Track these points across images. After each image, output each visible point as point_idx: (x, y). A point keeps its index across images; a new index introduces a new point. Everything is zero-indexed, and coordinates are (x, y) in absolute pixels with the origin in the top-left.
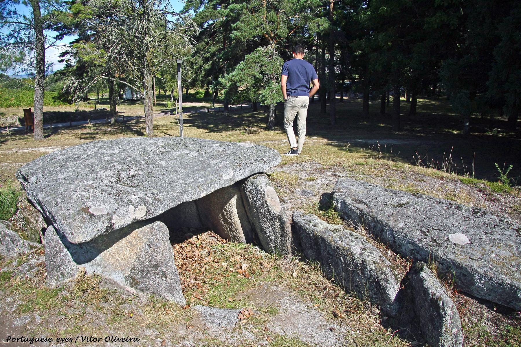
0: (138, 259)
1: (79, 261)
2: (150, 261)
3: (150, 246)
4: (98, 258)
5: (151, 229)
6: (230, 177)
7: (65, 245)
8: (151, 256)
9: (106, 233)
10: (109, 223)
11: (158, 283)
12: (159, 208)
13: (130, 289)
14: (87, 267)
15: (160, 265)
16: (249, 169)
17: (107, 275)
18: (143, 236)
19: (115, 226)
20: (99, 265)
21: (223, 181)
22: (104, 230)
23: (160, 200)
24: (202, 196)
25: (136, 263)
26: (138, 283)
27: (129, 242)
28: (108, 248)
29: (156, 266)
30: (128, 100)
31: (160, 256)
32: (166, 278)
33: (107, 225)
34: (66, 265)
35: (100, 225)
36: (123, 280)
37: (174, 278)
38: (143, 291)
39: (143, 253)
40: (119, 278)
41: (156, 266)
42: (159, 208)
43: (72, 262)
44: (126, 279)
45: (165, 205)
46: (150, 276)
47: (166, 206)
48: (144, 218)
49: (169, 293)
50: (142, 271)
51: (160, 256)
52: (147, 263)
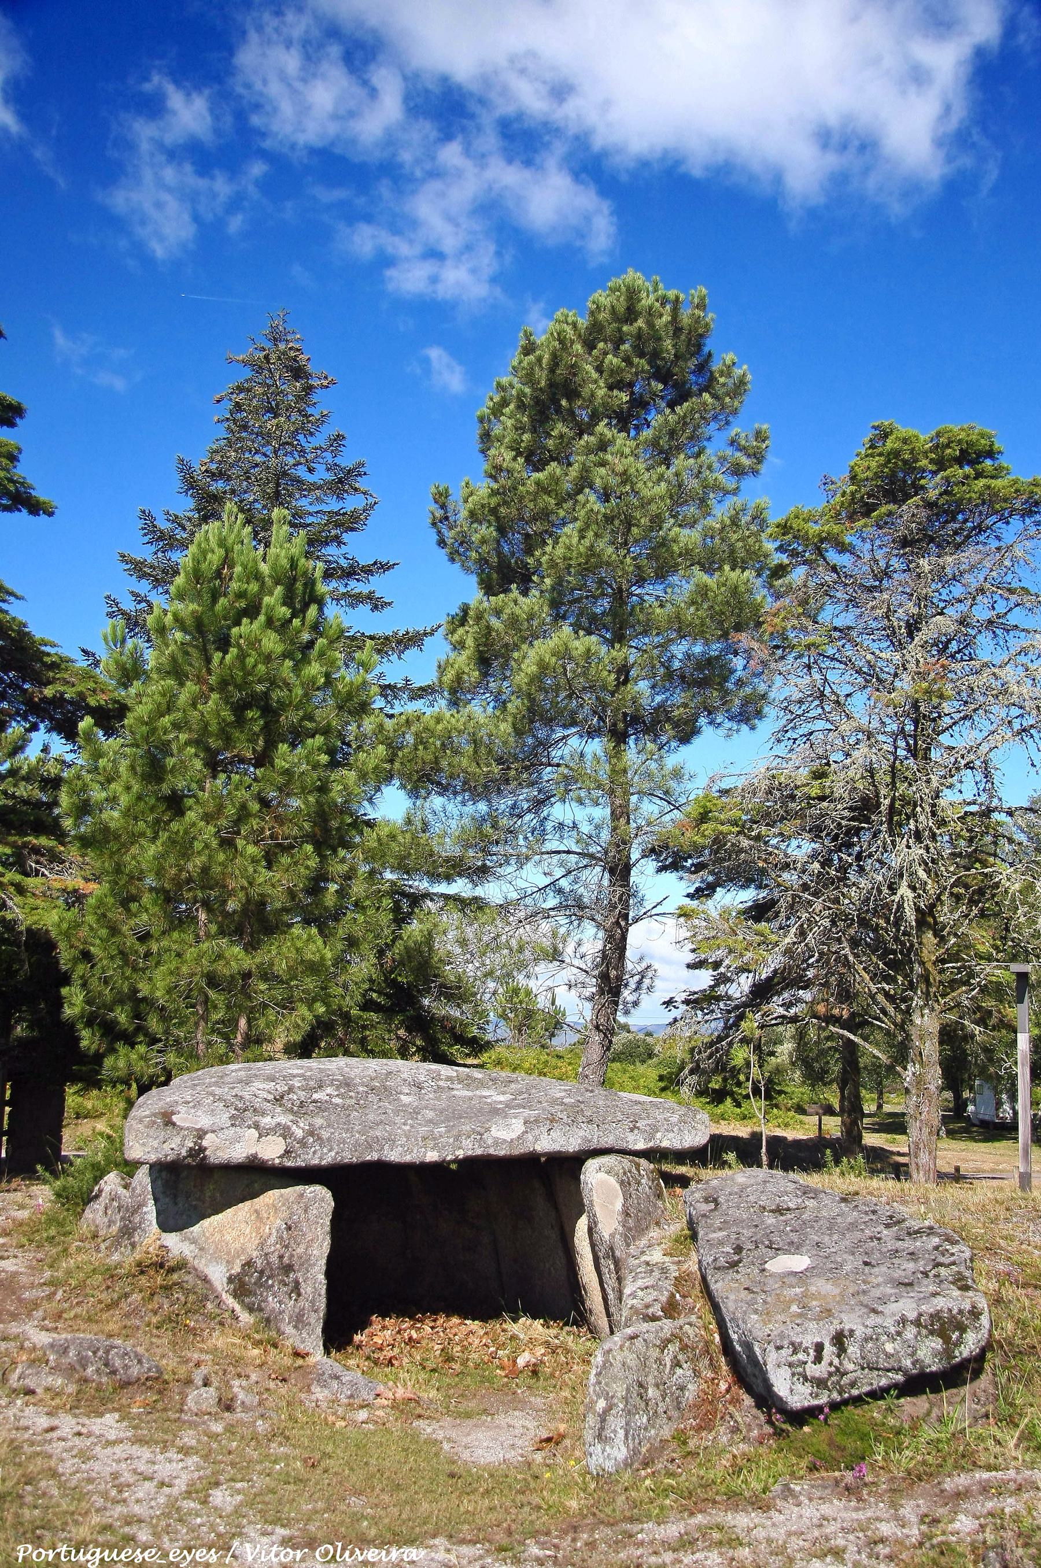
0: (262, 1245)
1: (166, 1226)
2: (281, 1257)
3: (289, 1228)
4: (196, 1229)
5: (301, 1195)
6: (514, 1136)
7: (153, 1194)
8: (287, 1247)
9: (190, 1160)
10: (195, 1143)
11: (280, 1302)
12: (314, 1153)
13: (230, 1301)
14: (172, 1240)
15: (296, 1267)
16: (582, 1133)
17: (201, 1265)
18: (284, 1205)
19: (207, 1153)
20: (194, 1241)
21: (490, 1142)
22: (184, 1153)
23: (320, 1138)
24: (428, 1159)
25: (255, 1254)
26: (250, 1293)
27: (256, 1211)
28: (217, 1212)
29: (288, 1269)
30: (984, 1124)
31: (300, 1250)
32: (299, 1295)
33: (191, 1145)
34: (144, 1230)
35: (178, 1140)
36: (225, 1280)
37: (313, 1302)
38: (251, 1309)
39: (273, 1239)
40: (218, 1275)
41: (288, 1269)
42: (314, 1153)
43: (155, 1227)
44: (230, 1280)
45: (330, 1150)
46: (273, 1286)
47: (333, 1154)
48: (277, 1161)
49: (295, 1327)
50: (262, 1272)
51: (300, 1250)
52: (274, 1259)
